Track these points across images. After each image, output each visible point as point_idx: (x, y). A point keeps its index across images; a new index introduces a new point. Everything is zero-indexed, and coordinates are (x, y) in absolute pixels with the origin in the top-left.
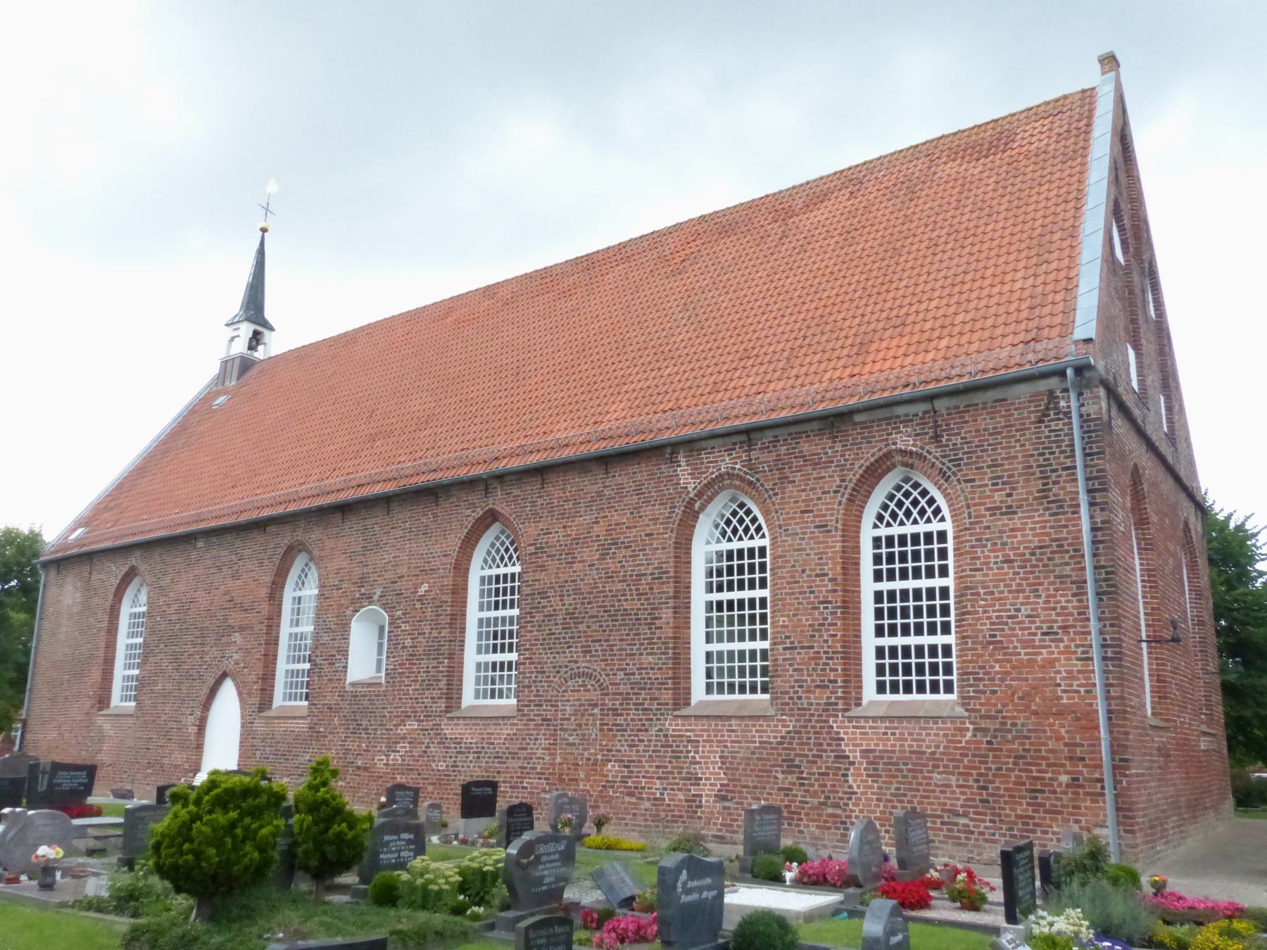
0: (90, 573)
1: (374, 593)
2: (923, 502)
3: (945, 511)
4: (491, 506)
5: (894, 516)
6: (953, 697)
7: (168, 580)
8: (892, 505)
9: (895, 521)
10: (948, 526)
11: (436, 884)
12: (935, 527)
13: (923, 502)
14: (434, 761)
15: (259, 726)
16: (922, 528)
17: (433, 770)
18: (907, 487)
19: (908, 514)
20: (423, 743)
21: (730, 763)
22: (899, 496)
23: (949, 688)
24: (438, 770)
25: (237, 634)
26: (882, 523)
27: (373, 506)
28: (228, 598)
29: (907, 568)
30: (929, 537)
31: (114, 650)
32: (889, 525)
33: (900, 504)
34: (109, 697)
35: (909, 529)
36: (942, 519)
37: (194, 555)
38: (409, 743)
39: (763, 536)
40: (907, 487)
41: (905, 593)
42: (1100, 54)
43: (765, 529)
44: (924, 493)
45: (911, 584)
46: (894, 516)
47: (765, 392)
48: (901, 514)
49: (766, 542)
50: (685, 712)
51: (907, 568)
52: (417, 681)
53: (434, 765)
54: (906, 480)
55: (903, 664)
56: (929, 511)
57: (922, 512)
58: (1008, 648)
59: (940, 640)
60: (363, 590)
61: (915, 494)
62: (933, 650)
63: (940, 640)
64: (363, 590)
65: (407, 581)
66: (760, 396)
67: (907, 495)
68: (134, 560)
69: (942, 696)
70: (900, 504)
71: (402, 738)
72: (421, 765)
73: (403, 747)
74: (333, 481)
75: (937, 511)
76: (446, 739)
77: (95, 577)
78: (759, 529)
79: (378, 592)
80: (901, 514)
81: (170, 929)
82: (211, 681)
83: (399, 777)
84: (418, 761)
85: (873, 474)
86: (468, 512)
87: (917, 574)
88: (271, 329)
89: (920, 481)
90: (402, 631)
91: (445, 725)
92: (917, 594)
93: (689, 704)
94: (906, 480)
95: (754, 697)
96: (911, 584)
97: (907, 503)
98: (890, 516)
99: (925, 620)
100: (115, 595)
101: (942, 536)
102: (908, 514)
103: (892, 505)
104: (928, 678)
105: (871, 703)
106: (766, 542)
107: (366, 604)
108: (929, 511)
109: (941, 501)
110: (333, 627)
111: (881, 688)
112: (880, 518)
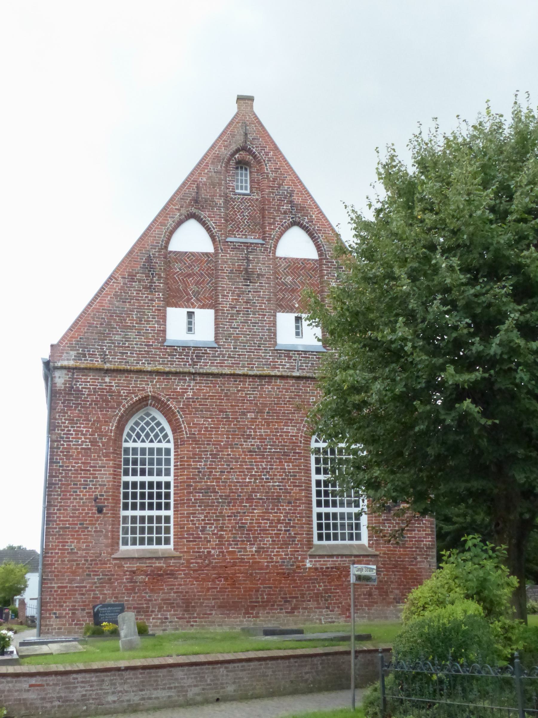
3: (171, 436)
9: (139, 439)
10: (171, 446)
11: (511, 213)
29: (144, 538)
36: (169, 441)
41: (143, 507)
42: (240, 94)
48: (143, 435)
51: (144, 538)
56: (161, 436)
57: (156, 436)
58: (199, 441)
59: (163, 479)
62: (159, 485)
63: (163, 513)
69: (163, 547)
70: (143, 429)
75: (166, 436)
80: (143, 435)
81: (381, 462)
89: (156, 416)
98: (145, 436)
101: (168, 485)
108: (161, 436)
112: (129, 436)
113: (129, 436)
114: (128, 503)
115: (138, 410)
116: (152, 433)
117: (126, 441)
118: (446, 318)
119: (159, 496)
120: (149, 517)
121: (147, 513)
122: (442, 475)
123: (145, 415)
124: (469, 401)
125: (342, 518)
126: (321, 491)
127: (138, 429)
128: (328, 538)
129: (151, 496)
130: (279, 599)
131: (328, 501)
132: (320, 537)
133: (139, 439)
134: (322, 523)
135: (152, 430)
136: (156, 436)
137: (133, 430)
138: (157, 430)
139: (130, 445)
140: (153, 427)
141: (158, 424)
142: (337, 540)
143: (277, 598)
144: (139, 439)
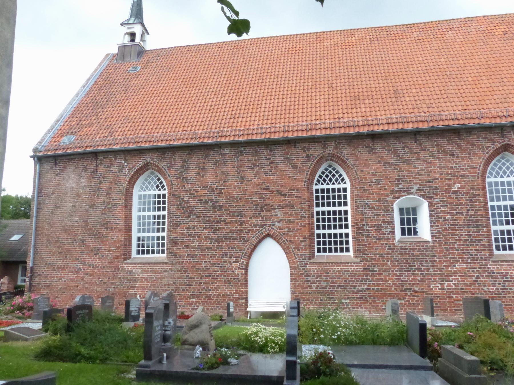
0: (97, 166)
1: (413, 188)
2: (337, 176)
4: (507, 142)
5: (324, 180)
6: (164, 255)
7: (192, 174)
8: (324, 176)
12: (342, 186)
13: (337, 176)
14: (485, 286)
15: (312, 269)
16: (336, 186)
17: (485, 291)
18: (330, 169)
19: (330, 180)
20: (474, 276)
21: (358, 281)
22: (327, 173)
23: (163, 252)
24: (490, 292)
25: (277, 210)
26: (331, 182)
27: (402, 137)
28: (263, 187)
30: (339, 190)
31: (131, 219)
32: (322, 184)
33: (327, 176)
34: (130, 252)
35: (331, 186)
37: (219, 158)
38: (460, 276)
39: (165, 190)
40: (330, 169)
43: (166, 187)
44: (337, 172)
45: (332, 209)
46: (324, 180)
47: (150, 133)
48: (327, 180)
49: (166, 192)
50: (128, 261)
52: (461, 240)
53: (485, 289)
54: (330, 166)
55: (323, 241)
56: (340, 180)
57: (337, 180)
60: (400, 186)
61: (334, 172)
64: (400, 186)
65: (440, 182)
66: (148, 135)
67: (330, 172)
68: (151, 158)
69: (160, 255)
70: (327, 176)
71: (454, 273)
72: (473, 289)
73: (455, 280)
74: (347, 119)
75: (343, 180)
76: (494, 273)
77: (100, 169)
78: (163, 187)
79: (416, 187)
80: (327, 180)
82: (255, 241)
83: (454, 296)
84: (471, 286)
85: (319, 163)
86: (488, 144)
87: (334, 204)
88: (148, 34)
89: (336, 167)
90: (441, 211)
91: (490, 265)
92: (334, 213)
93: (130, 258)
94: (330, 166)
95: (342, 254)
96: (332, 209)
97: (330, 176)
98: (496, 173)
99: (332, 223)
100: (129, 182)
102: (330, 180)
103: (324, 176)
104: (327, 246)
105: (134, 258)
106: (166, 192)
107: (405, 194)
108: (340, 180)
109: (345, 176)
110: (376, 207)
111: (138, 252)
112: (318, 181)
113: (491, 174)
115: (498, 154)
117: (489, 177)
119: (340, 220)
121: (332, 231)
123: (500, 158)
127: (497, 169)
129: (335, 220)
130: (126, 281)
134: (405, 228)
135: (334, 176)
137: (493, 169)
139: (493, 180)
140: (337, 174)
141: (323, 173)
142: (411, 235)
143: (124, 280)
144: (331, 182)
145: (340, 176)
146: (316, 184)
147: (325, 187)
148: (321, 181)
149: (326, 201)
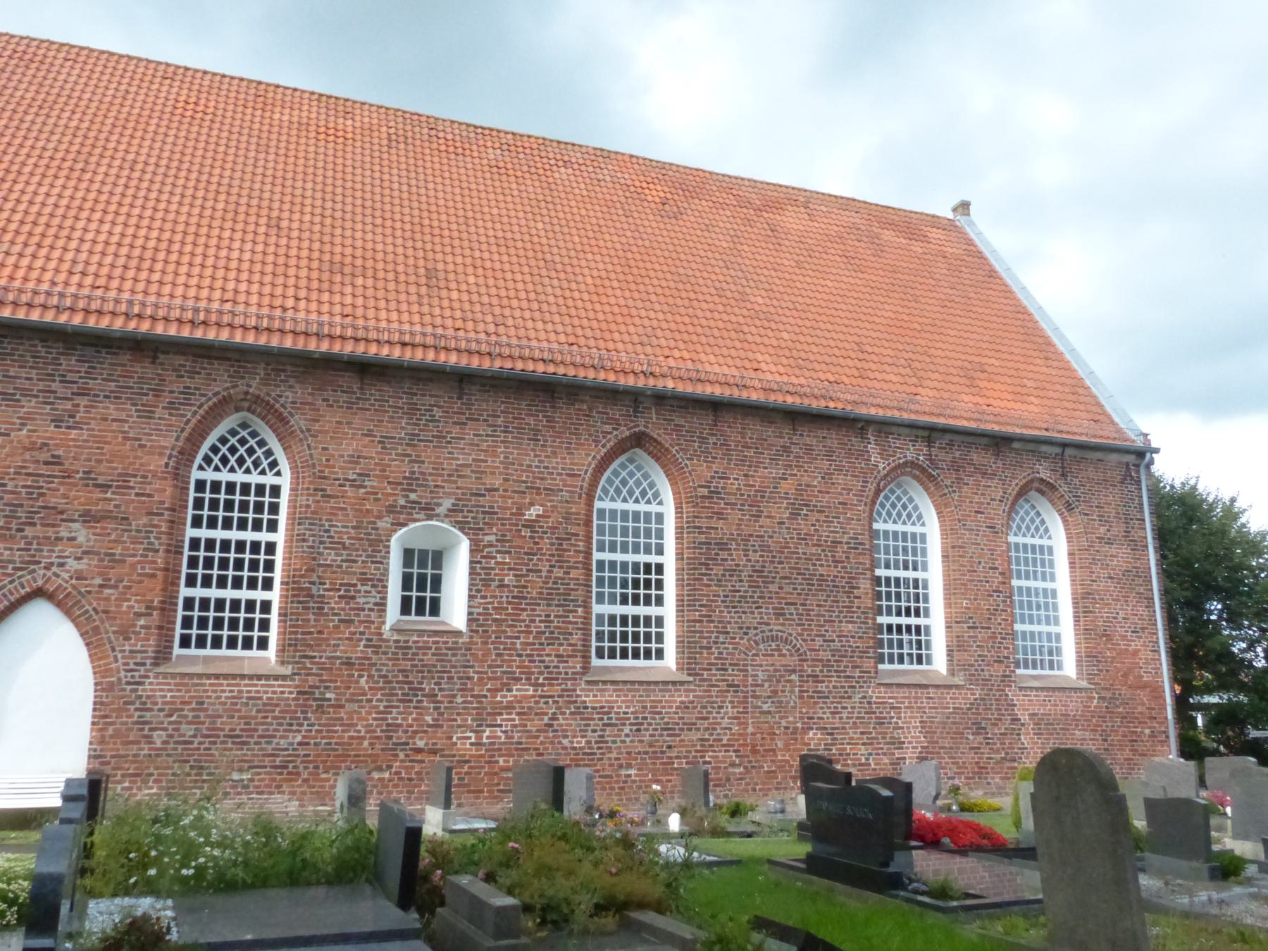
5: (224, 460)
36: (278, 474)
46: (224, 460)
48: (233, 461)
56: (265, 464)
57: (644, 493)
70: (233, 450)
75: (274, 464)
113: (605, 491)
114: (213, 558)
116: (233, 455)
117: (601, 499)
118: (1196, 531)
120: (610, 562)
122: (136, 882)
124: (92, 904)
125: (898, 585)
126: (411, 597)
127: (617, 482)
128: (201, 642)
131: (638, 595)
132: (185, 642)
133: (225, 466)
136: (644, 493)
137: (610, 482)
138: (645, 484)
144: (225, 466)
145: (269, 453)
146: (201, 468)
147: (224, 476)
148: (216, 460)
149: (236, 515)
